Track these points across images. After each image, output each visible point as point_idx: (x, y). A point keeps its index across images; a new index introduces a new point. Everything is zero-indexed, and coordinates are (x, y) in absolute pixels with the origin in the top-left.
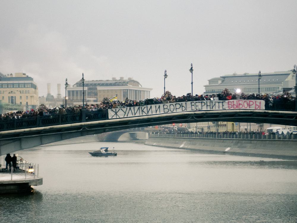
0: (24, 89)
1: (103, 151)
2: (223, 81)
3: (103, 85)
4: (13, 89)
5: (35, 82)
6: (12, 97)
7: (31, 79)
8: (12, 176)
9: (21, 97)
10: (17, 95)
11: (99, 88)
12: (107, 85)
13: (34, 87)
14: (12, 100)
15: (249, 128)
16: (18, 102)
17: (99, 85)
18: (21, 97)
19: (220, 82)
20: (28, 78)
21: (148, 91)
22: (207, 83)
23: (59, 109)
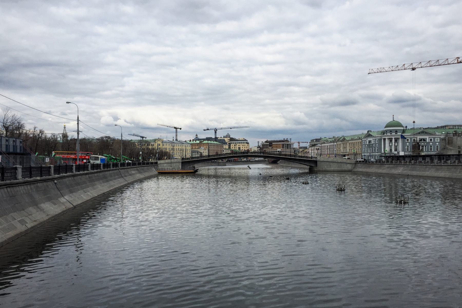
0: (244, 144)
1: (241, 169)
2: (316, 141)
3: (275, 142)
4: (240, 145)
5: (248, 141)
6: (239, 147)
7: (247, 141)
8: (122, 138)
9: (242, 147)
10: (241, 146)
11: (273, 143)
12: (278, 142)
13: (248, 143)
14: (239, 148)
15: (332, 169)
16: (241, 149)
17: (273, 142)
18: (242, 147)
19: (315, 141)
20: (245, 140)
21: (384, 139)
22: (310, 141)
23: (155, 153)
